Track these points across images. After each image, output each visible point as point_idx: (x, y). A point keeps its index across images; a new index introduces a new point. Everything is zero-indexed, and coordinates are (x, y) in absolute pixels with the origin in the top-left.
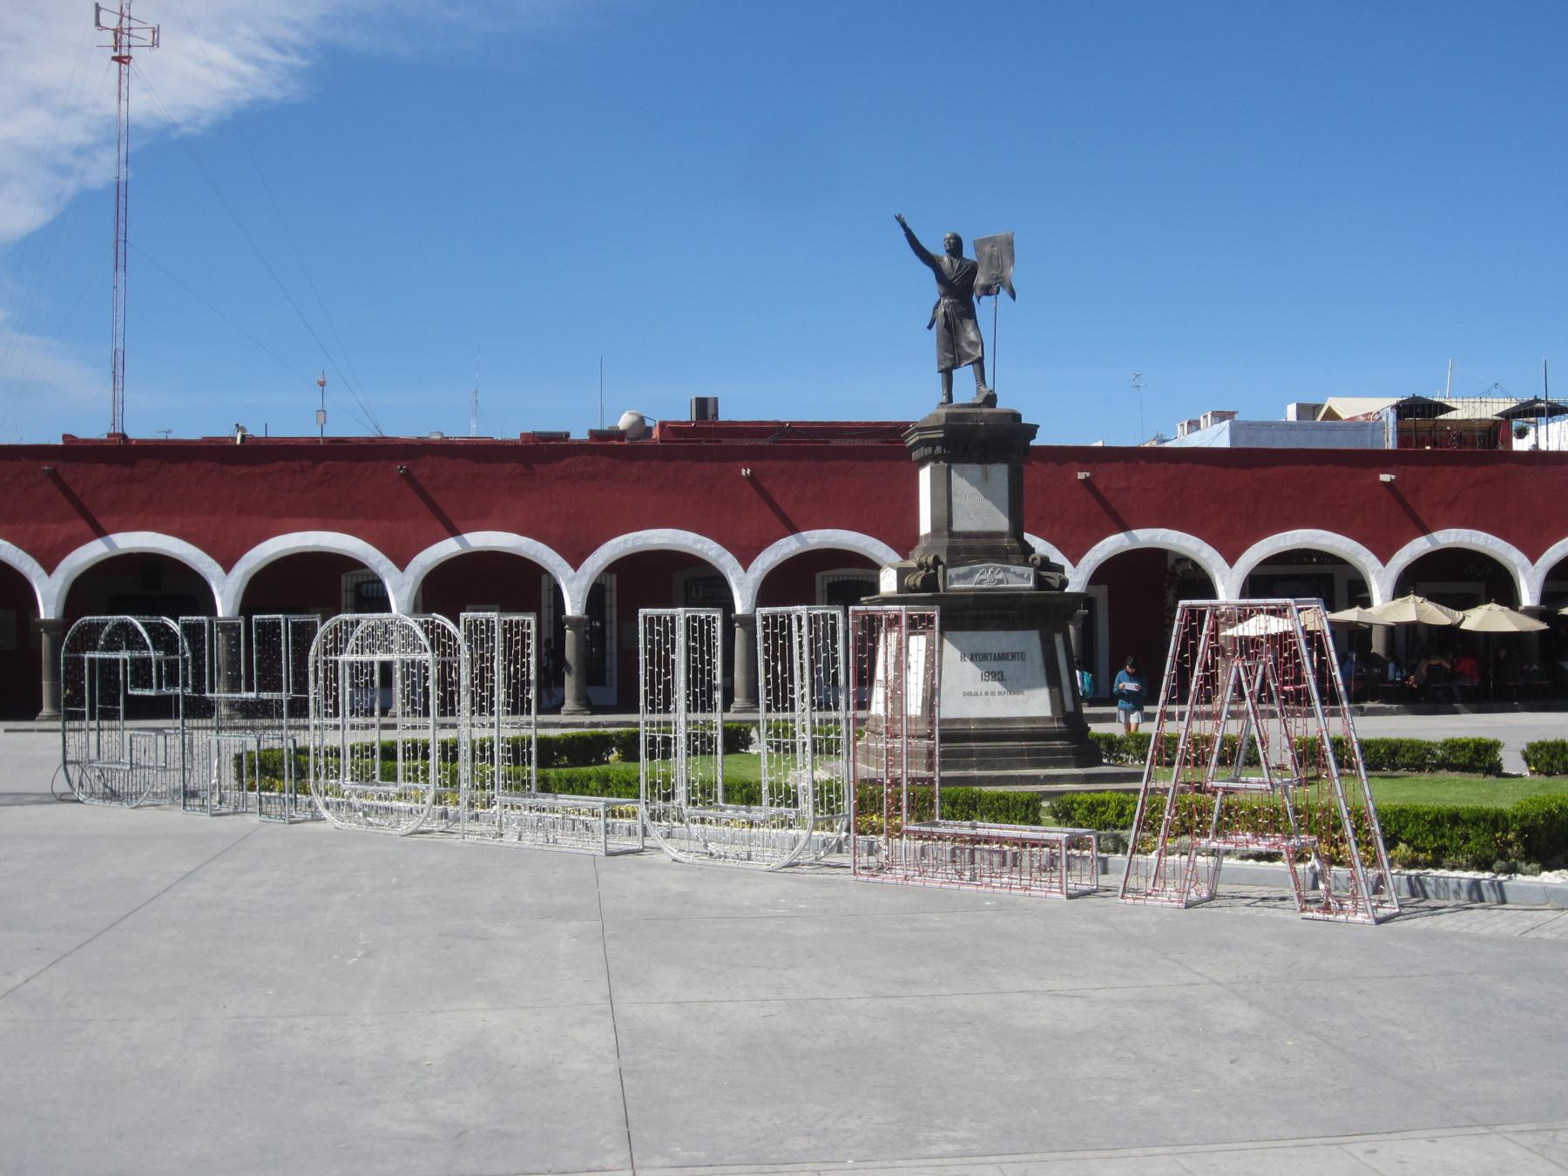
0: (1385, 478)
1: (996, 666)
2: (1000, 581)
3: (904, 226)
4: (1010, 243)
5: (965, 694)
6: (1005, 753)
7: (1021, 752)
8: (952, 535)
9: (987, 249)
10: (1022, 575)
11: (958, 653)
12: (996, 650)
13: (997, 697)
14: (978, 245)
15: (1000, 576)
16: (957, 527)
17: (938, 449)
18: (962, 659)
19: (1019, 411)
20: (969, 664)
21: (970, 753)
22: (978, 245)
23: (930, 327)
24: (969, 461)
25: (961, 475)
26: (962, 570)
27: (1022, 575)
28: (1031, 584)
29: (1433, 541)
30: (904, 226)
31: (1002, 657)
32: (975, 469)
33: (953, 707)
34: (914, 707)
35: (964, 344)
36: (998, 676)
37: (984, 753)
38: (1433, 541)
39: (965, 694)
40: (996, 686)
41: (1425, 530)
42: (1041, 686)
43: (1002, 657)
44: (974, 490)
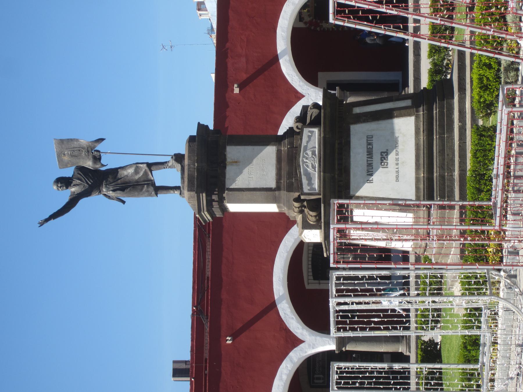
1: (376, 157)
2: (313, 153)
3: (47, 220)
4: (62, 141)
5: (397, 179)
6: (442, 151)
8: (278, 188)
10: (309, 137)
11: (367, 185)
14: (63, 165)
15: (310, 153)
16: (273, 185)
17: (215, 197)
18: (371, 182)
20: (376, 177)
21: (442, 177)
22: (63, 165)
23: (124, 202)
24: (223, 175)
25: (234, 181)
27: (309, 137)
28: (316, 130)
30: (47, 220)
31: (370, 153)
32: (230, 170)
37: (442, 167)
39: (397, 179)
40: (391, 157)
42: (392, 124)
43: (370, 153)
44: (246, 171)
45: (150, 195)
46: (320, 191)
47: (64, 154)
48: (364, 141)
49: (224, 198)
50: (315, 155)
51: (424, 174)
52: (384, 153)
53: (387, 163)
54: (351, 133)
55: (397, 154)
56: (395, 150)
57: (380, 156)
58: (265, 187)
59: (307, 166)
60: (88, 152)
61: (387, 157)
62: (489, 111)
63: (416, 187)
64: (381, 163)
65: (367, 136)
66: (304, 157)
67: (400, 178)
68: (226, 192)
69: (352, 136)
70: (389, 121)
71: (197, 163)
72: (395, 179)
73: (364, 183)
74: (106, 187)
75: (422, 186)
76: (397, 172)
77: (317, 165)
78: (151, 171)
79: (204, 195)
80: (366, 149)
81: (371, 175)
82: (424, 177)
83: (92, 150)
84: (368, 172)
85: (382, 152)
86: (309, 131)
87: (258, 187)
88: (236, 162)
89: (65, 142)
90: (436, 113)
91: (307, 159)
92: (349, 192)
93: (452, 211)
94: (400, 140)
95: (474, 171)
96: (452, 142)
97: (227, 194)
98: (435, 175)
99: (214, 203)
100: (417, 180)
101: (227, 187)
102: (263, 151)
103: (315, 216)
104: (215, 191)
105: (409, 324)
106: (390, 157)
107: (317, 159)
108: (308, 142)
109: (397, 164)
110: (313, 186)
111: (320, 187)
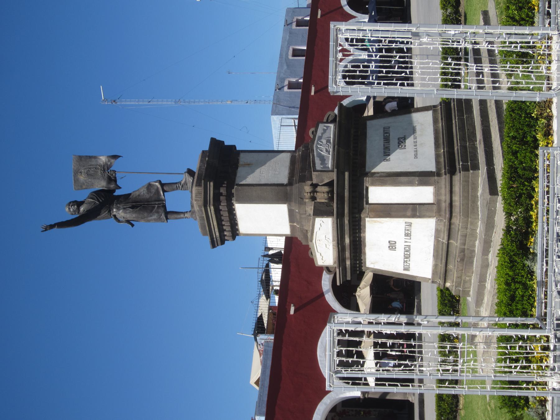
0: (292, 312)
1: (393, 142)
2: (328, 141)
3: (52, 227)
4: (80, 158)
5: (416, 156)
6: (462, 128)
7: (461, 121)
8: (290, 183)
9: (82, 178)
10: (325, 131)
11: (383, 163)
12: (382, 142)
13: (418, 140)
14: (79, 186)
15: (324, 141)
16: (285, 181)
17: (223, 190)
18: (389, 160)
19: (200, 152)
20: (393, 157)
21: (464, 147)
22: (79, 186)
23: (133, 225)
24: (235, 175)
25: (245, 178)
26: (318, 161)
27: (325, 131)
28: (332, 126)
29: (328, 291)
30: (52, 227)
31: (387, 139)
32: (241, 171)
33: (428, 163)
34: (424, 194)
35: (147, 196)
36: (401, 141)
37: (463, 139)
38: (328, 291)
39: (416, 156)
40: (409, 142)
41: (322, 295)
42: (411, 118)
43: (387, 139)
44: (258, 171)
45: (159, 219)
46: (333, 168)
47: (81, 173)
48: (382, 131)
49: (233, 194)
50: (330, 143)
51: (444, 149)
52: (402, 138)
53: (405, 146)
54: (368, 127)
55: (415, 138)
56: (413, 136)
57: (397, 141)
58: (276, 183)
59: (321, 151)
60: (104, 170)
61: (405, 141)
62: (452, 313)
63: (436, 161)
64: (399, 146)
65: (384, 128)
66: (318, 143)
67: (418, 156)
68: (235, 187)
69: (368, 129)
70: (407, 115)
71: (208, 157)
72: (414, 156)
73: (381, 162)
74: (117, 204)
75: (442, 160)
76: (416, 151)
77: (331, 150)
78: (164, 191)
79: (212, 184)
80: (382, 137)
81: (389, 155)
82: (444, 152)
83: (108, 169)
84: (385, 153)
85: (399, 138)
86: (325, 126)
87: (270, 183)
88: (249, 164)
89: (83, 159)
90: (454, 104)
91: (321, 145)
92: (365, 170)
93: (476, 172)
94: (418, 128)
95: (476, 219)
96: (472, 121)
97: (237, 190)
98: (456, 149)
99: (222, 198)
100: (437, 156)
101: (237, 182)
102: (278, 157)
103: (328, 193)
104: (224, 184)
105: (483, 77)
106: (407, 141)
107: (331, 146)
108: (322, 134)
109: (416, 146)
110: (327, 166)
111: (333, 165)
